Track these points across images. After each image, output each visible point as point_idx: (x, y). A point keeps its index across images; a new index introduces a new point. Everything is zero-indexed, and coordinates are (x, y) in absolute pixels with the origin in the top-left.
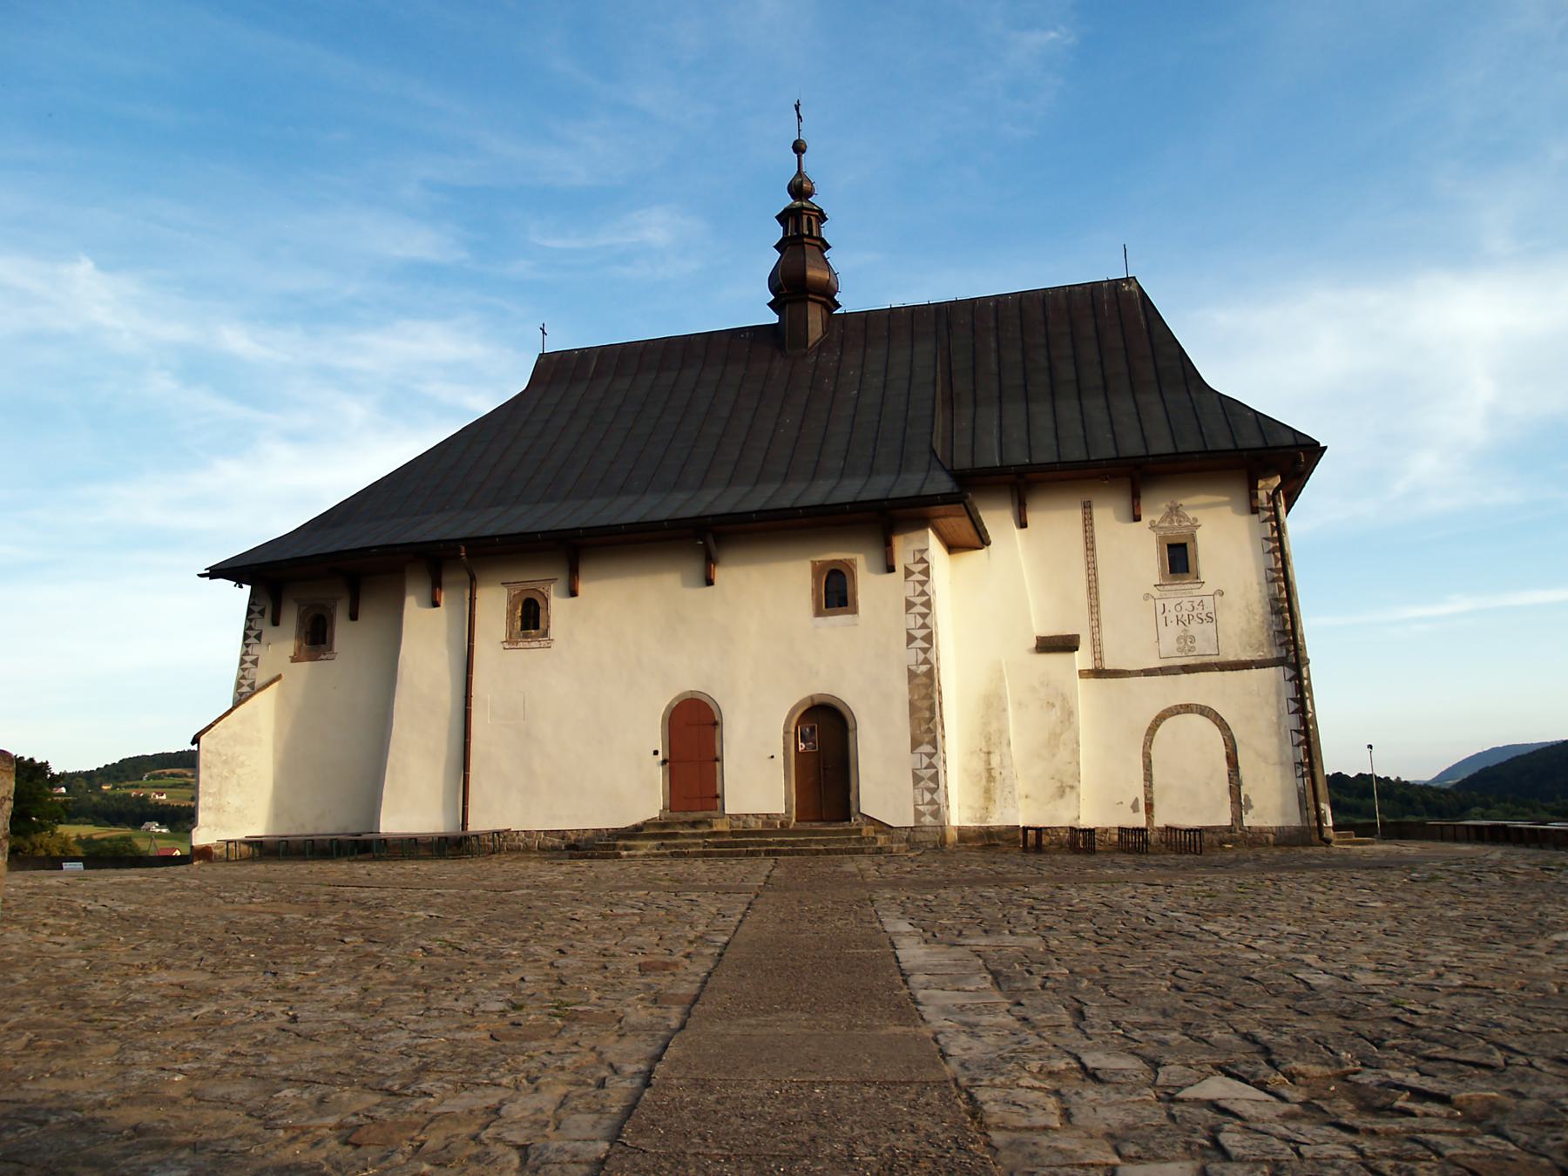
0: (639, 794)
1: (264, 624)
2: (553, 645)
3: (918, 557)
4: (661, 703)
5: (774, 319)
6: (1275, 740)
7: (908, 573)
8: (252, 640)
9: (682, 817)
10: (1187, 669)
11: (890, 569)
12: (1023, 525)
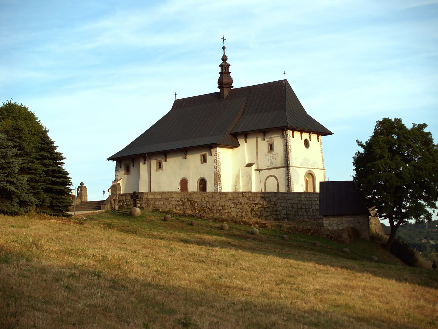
1: (119, 168)
4: (179, 180)
5: (218, 90)
6: (284, 181)
7: (214, 156)
10: (271, 169)
11: (211, 155)
12: (246, 142)
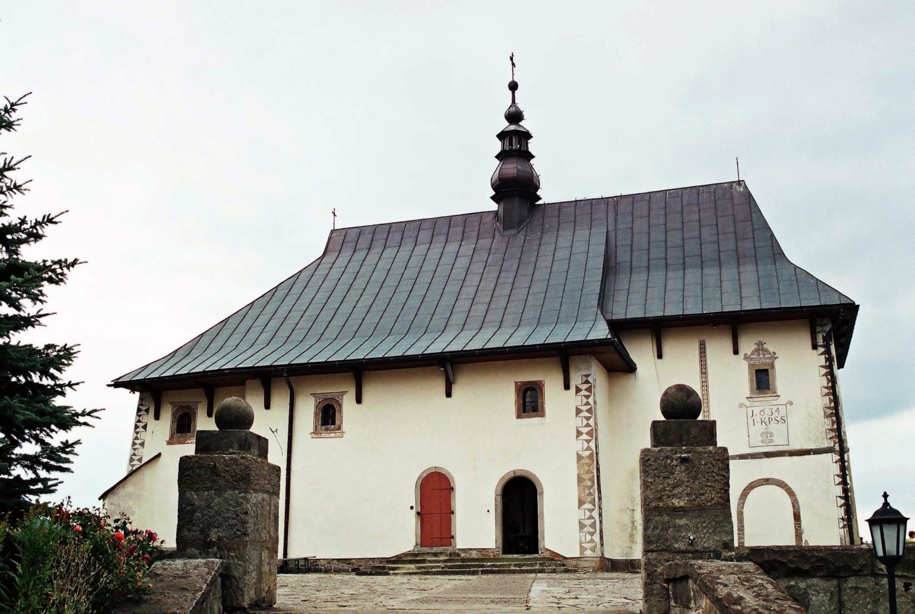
0: (403, 536)
1: (149, 419)
2: (345, 435)
3: (584, 379)
7: (578, 390)
8: (140, 429)
9: (428, 550)
10: (768, 455)
11: (736, 352)
